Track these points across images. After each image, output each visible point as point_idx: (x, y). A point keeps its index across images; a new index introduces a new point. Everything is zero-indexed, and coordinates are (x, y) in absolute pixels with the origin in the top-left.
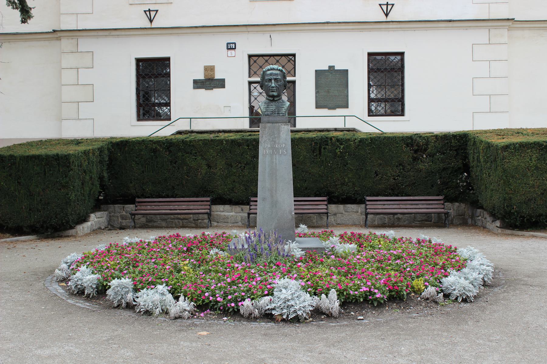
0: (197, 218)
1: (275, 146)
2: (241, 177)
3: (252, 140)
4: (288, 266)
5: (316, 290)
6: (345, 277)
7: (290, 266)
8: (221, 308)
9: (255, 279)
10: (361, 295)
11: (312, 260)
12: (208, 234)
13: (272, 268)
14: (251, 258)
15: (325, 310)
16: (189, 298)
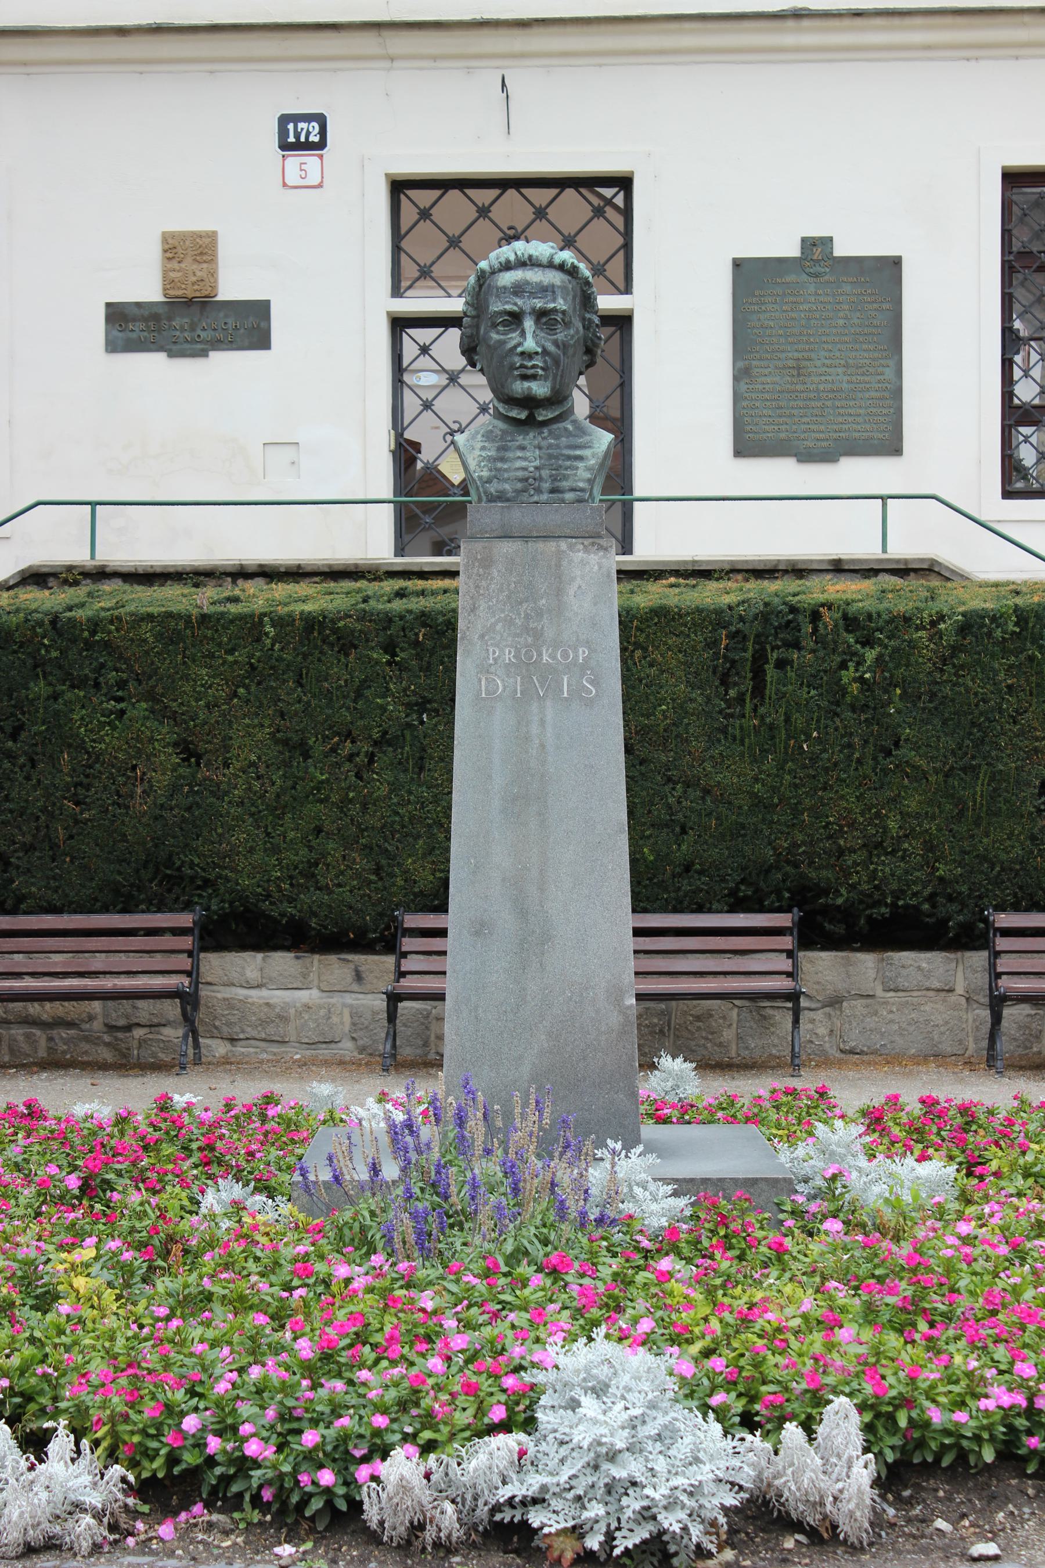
0: (127, 1017)
1: (540, 655)
2: (355, 810)
3: (409, 617)
4: (605, 1272)
5: (753, 1399)
6: (900, 1331)
7: (616, 1275)
8: (267, 1494)
9: (438, 1345)
10: (983, 1428)
11: (726, 1244)
12: (190, 1104)
13: (524, 1283)
14: (420, 1233)
15: (801, 1507)
16: (96, 1443)
